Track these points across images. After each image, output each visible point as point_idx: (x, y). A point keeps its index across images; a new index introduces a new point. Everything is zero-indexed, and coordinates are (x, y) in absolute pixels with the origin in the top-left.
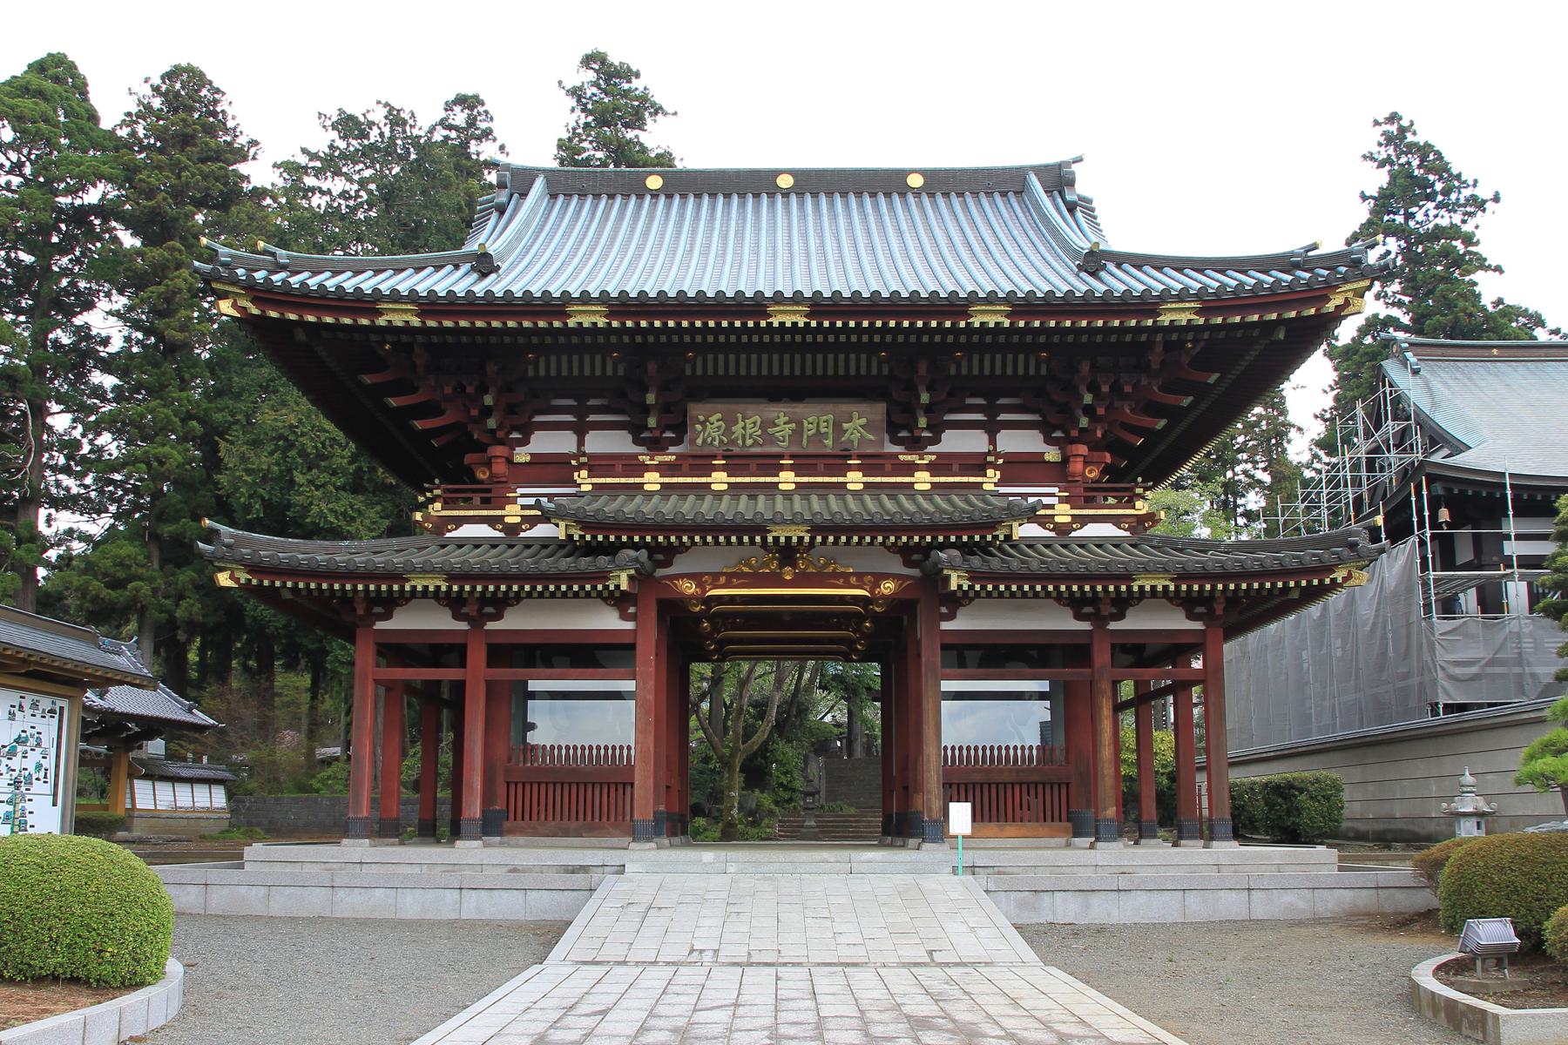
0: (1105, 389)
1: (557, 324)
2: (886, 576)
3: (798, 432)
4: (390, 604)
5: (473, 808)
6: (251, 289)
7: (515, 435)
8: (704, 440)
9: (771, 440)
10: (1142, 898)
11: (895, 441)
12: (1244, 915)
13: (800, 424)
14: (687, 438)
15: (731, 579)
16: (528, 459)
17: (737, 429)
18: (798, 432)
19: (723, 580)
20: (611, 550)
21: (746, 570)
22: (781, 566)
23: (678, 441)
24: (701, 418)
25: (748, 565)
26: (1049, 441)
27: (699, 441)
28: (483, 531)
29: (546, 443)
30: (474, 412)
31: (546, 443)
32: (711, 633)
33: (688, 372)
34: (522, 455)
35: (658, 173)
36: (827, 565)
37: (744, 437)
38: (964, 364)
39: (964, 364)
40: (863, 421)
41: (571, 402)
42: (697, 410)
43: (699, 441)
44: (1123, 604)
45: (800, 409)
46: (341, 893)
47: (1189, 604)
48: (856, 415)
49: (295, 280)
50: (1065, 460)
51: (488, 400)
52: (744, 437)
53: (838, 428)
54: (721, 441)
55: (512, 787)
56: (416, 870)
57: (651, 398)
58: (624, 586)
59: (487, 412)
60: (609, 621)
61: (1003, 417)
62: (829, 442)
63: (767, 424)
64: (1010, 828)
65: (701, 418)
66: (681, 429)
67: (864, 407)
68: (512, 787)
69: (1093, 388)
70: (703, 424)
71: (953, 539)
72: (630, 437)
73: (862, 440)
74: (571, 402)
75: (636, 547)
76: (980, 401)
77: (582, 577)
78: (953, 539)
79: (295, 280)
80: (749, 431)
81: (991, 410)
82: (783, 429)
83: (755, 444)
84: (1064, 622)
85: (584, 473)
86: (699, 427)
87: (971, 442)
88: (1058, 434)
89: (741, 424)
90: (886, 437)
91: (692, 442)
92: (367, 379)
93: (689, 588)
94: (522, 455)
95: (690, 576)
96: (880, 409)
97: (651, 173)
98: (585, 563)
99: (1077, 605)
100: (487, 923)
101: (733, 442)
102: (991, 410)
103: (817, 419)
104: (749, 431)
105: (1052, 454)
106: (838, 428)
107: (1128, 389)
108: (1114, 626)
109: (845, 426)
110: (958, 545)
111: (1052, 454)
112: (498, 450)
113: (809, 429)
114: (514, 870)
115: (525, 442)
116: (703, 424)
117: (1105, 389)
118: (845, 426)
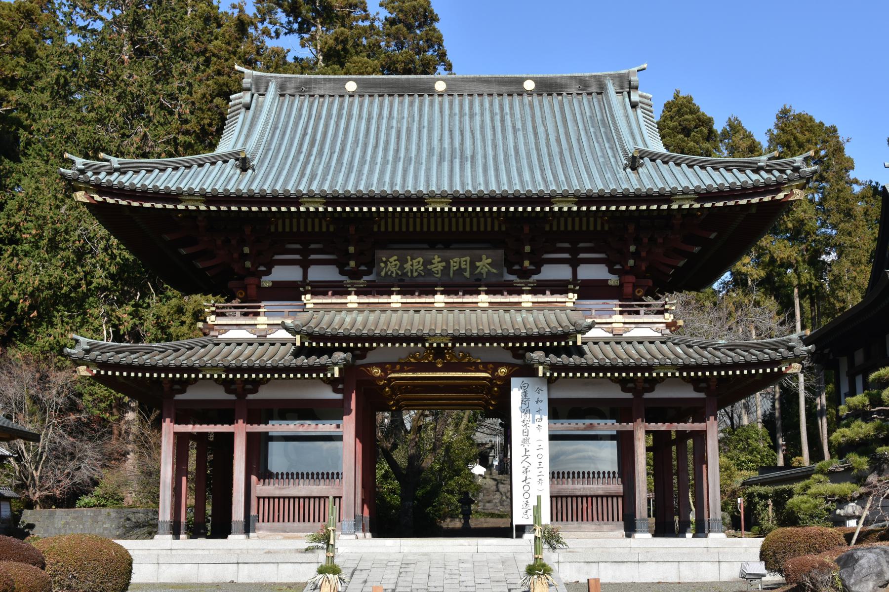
0: (646, 240)
1: (293, 209)
2: (502, 365)
3: (447, 268)
4: (184, 385)
5: (238, 513)
6: (100, 189)
7: (262, 268)
8: (386, 273)
9: (429, 273)
10: (654, 566)
11: (511, 272)
12: (677, 581)
13: (448, 263)
14: (375, 270)
15: (404, 366)
16: (271, 284)
17: (408, 266)
18: (447, 268)
19: (398, 367)
20: (330, 352)
21: (413, 360)
22: (435, 358)
23: (369, 273)
24: (384, 259)
25: (414, 357)
26: (611, 271)
27: (383, 274)
28: (243, 334)
29: (284, 273)
30: (236, 255)
31: (284, 273)
32: (391, 396)
33: (376, 229)
34: (266, 281)
35: (354, 80)
36: (464, 357)
37: (412, 271)
38: (555, 223)
39: (555, 223)
40: (489, 261)
41: (298, 246)
42: (382, 255)
43: (383, 274)
44: (652, 383)
45: (448, 253)
46: (164, 567)
47: (696, 383)
48: (484, 257)
49: (124, 179)
50: (621, 285)
51: (246, 250)
52: (412, 271)
53: (473, 266)
54: (397, 274)
55: (261, 500)
56: (207, 552)
57: (351, 249)
58: (337, 375)
59: (245, 257)
60: (328, 394)
61: (582, 256)
62: (467, 274)
63: (427, 262)
64: (586, 525)
65: (384, 259)
66: (371, 265)
67: (489, 252)
68: (261, 500)
69: (637, 241)
70: (385, 263)
71: (540, 344)
72: (337, 270)
73: (488, 273)
74: (298, 246)
75: (345, 350)
76: (567, 245)
77: (311, 369)
78: (540, 344)
79: (124, 179)
80: (415, 268)
81: (574, 251)
82: (437, 265)
83: (420, 275)
84: (616, 393)
85: (308, 296)
86: (382, 265)
87: (562, 272)
88: (618, 267)
89: (410, 263)
90: (505, 270)
91: (378, 274)
92: (167, 238)
93: (377, 372)
94: (266, 281)
95: (378, 365)
96: (501, 252)
97: (350, 80)
98: (314, 360)
99: (624, 384)
100: (147, 584)
101: (405, 274)
102: (574, 251)
103: (460, 261)
104: (415, 268)
105: (613, 280)
106: (473, 266)
107: (660, 240)
108: (647, 395)
109: (478, 264)
110: (543, 349)
111: (613, 280)
112: (251, 280)
113: (454, 264)
114: (269, 552)
115: (268, 273)
116: (385, 263)
117: (646, 240)
118: (478, 264)
